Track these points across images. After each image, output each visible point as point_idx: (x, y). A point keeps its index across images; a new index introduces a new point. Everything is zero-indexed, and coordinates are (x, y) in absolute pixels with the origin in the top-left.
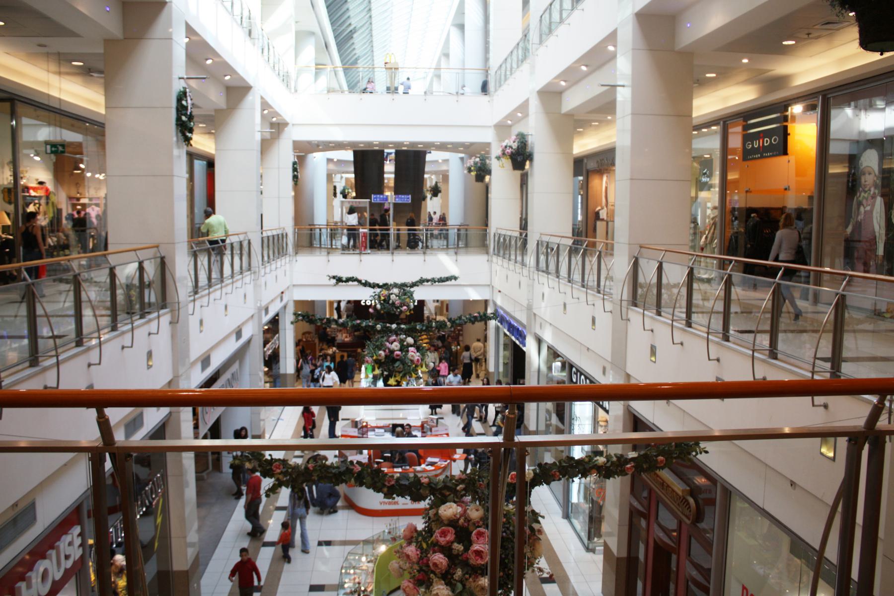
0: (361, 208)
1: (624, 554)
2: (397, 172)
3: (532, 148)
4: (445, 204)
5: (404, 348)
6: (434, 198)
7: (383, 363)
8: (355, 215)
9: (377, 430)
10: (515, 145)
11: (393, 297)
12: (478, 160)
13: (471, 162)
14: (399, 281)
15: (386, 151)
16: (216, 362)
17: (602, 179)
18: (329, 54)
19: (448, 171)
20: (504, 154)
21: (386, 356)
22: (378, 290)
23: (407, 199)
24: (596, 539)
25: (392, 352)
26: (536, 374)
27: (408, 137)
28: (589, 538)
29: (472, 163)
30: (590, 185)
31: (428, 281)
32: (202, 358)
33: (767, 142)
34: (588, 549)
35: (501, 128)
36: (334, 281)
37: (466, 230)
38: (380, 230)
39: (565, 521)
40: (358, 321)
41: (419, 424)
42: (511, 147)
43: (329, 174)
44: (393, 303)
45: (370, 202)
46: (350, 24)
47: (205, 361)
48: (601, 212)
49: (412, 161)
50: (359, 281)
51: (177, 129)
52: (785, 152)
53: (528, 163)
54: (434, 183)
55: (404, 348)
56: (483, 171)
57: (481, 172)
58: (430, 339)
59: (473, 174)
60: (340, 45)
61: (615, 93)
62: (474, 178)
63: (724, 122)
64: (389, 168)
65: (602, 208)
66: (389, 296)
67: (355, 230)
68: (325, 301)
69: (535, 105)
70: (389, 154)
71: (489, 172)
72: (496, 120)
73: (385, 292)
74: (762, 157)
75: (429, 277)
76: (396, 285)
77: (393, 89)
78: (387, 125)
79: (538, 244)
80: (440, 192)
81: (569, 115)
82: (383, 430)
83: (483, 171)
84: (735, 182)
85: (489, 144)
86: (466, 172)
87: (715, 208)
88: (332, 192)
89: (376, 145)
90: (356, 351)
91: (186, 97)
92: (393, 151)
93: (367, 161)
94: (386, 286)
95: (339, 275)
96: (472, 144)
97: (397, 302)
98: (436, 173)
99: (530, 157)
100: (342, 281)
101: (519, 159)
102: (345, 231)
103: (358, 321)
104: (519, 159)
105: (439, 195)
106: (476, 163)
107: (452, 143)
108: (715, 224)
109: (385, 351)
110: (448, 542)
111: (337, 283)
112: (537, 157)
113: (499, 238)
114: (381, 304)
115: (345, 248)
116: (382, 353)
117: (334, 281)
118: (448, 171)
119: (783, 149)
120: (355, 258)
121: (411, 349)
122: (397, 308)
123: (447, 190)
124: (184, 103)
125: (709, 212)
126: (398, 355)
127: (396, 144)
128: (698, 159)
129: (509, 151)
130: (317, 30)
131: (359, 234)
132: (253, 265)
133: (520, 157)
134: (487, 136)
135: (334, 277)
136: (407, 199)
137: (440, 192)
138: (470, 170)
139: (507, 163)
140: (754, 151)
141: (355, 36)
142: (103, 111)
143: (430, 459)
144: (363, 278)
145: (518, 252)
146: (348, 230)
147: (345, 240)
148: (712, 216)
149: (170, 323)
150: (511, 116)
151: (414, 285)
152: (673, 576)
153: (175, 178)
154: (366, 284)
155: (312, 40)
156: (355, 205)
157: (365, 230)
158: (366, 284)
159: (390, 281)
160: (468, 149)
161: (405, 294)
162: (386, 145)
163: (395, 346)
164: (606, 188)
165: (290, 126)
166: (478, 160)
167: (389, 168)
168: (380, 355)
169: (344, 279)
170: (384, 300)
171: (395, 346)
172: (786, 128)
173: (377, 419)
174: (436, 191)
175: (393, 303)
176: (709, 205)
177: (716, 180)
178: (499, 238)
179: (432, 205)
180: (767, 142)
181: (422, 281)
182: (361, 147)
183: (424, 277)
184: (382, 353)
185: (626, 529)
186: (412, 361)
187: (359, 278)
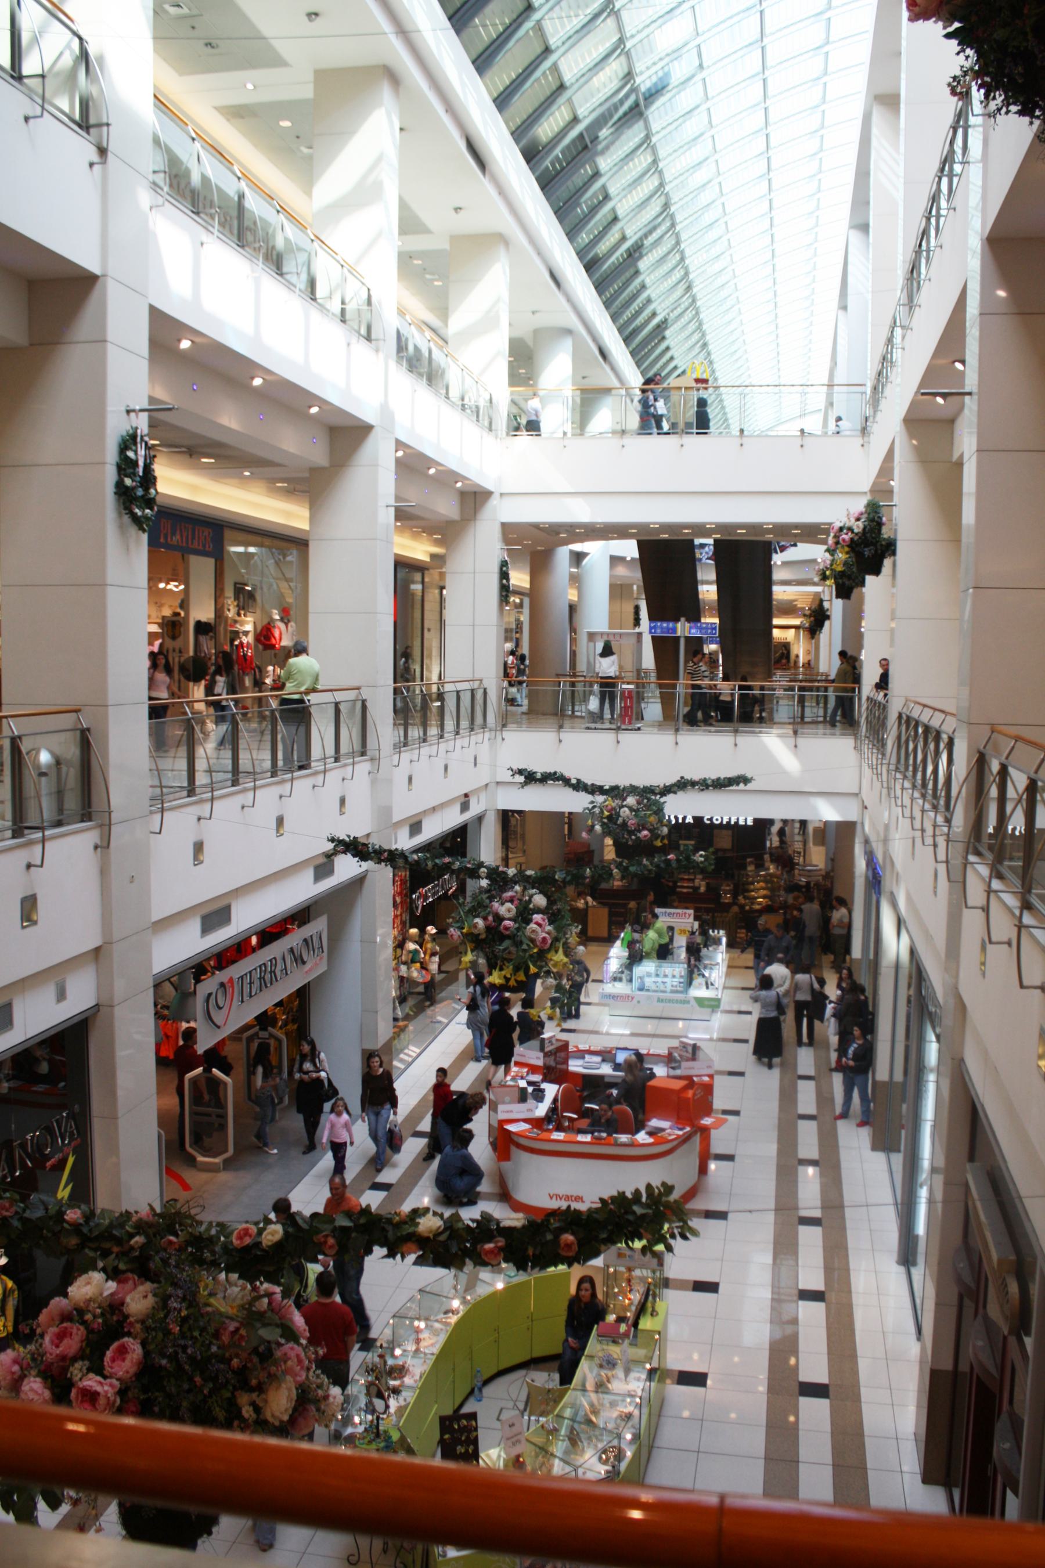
5: (524, 915)
7: (483, 940)
9: (588, 1057)
14: (641, 782)
15: (697, 541)
16: (248, 916)
18: (613, 369)
21: (488, 928)
22: (600, 799)
26: (893, 971)
31: (693, 784)
32: (206, 910)
36: (522, 779)
39: (902, 1269)
40: (447, 860)
41: (665, 1052)
42: (850, 529)
43: (598, 582)
44: (624, 824)
46: (654, 314)
47: (215, 916)
49: (746, 558)
50: (567, 782)
51: (118, 500)
55: (524, 915)
58: (772, 890)
68: (563, 813)
70: (702, 546)
73: (612, 803)
75: (696, 778)
76: (633, 790)
80: (828, 617)
82: (598, 1059)
89: (768, 531)
90: (625, 905)
91: (135, 444)
92: (711, 541)
93: (665, 563)
94: (615, 792)
95: (532, 767)
97: (632, 822)
100: (536, 780)
101: (867, 552)
102: (596, 687)
103: (447, 860)
104: (867, 552)
109: (485, 919)
110: (63, 1358)
111: (523, 785)
114: (603, 825)
115: (597, 717)
117: (522, 779)
120: (609, 737)
121: (537, 917)
122: (631, 833)
124: (130, 454)
126: (507, 928)
129: (846, 537)
132: (369, 745)
135: (520, 772)
141: (667, 333)
143: (655, 1123)
144: (572, 774)
146: (602, 685)
147: (594, 704)
149: (96, 847)
151: (667, 790)
153: (110, 589)
154: (579, 786)
155: (568, 343)
158: (579, 786)
159: (623, 782)
161: (648, 807)
162: (701, 529)
163: (506, 909)
165: (494, 501)
168: (475, 926)
169: (539, 776)
170: (609, 818)
171: (506, 909)
173: (633, 1035)
175: (624, 824)
181: (682, 785)
183: (688, 777)
184: (480, 922)
186: (533, 941)
187: (567, 774)
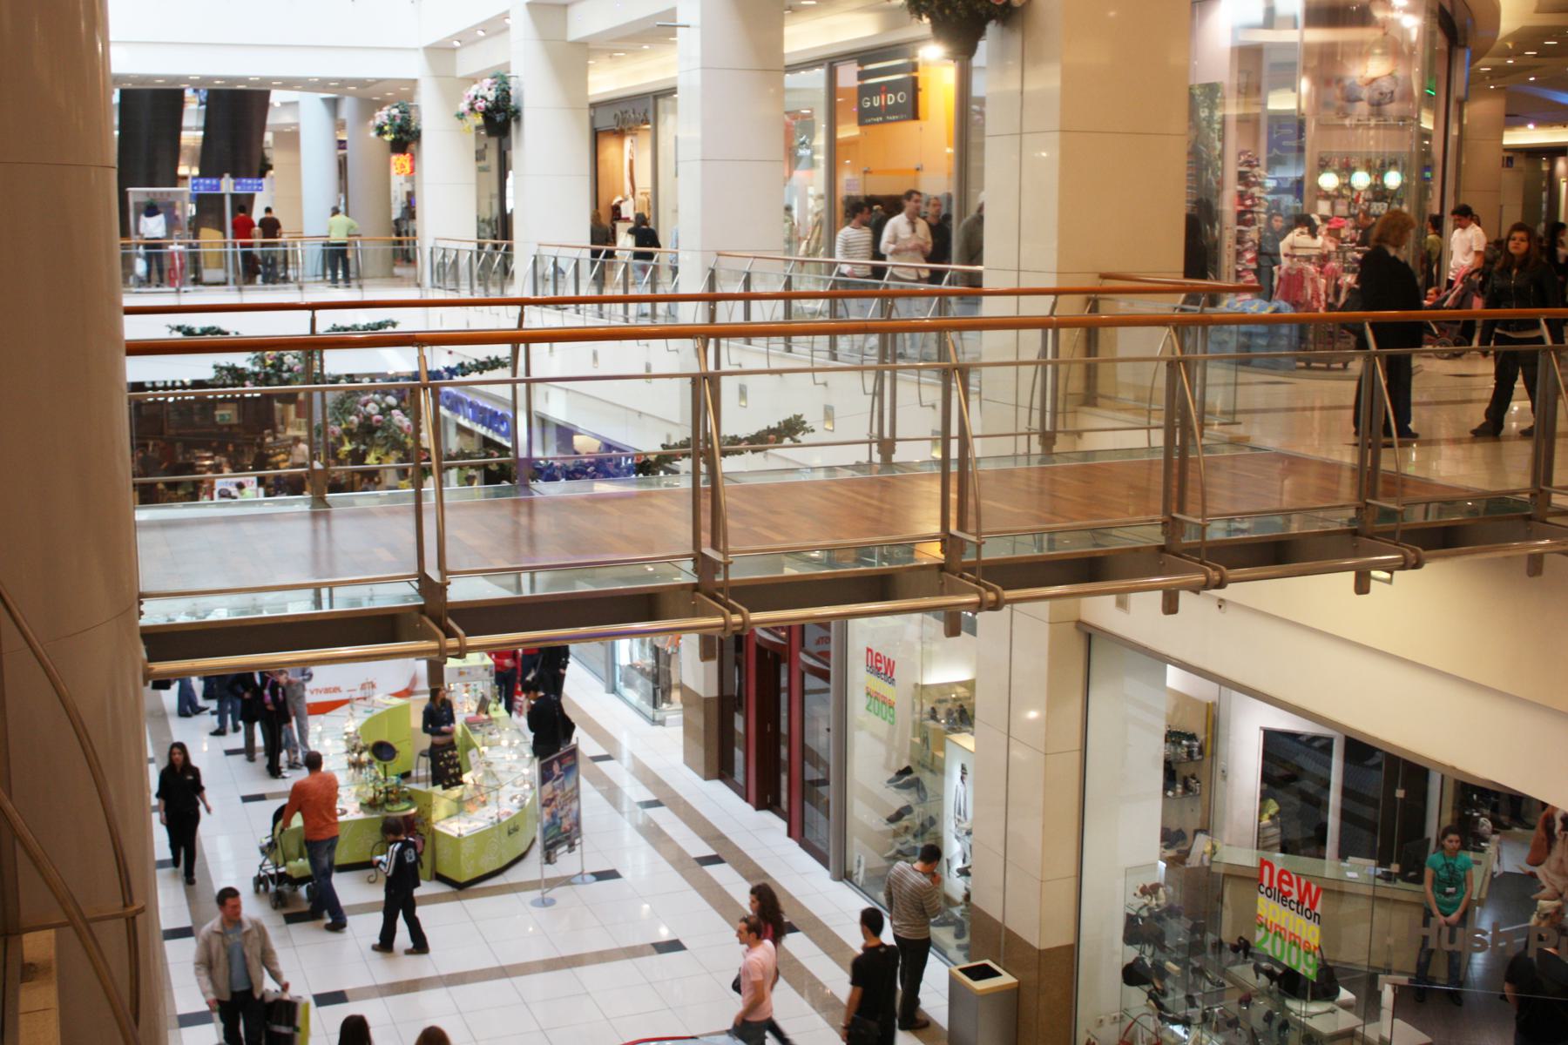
1: (714, 693)
2: (177, 128)
3: (519, 98)
10: (491, 95)
13: (381, 116)
17: (622, 146)
20: (472, 109)
24: (665, 705)
25: (368, 417)
28: (655, 705)
30: (601, 157)
33: (891, 99)
34: (654, 722)
35: (440, 53)
38: (263, 245)
39: (612, 696)
42: (484, 98)
48: (623, 206)
52: (915, 116)
57: (405, 138)
62: (388, 147)
63: (831, 64)
65: (626, 199)
67: (159, 246)
74: (885, 121)
79: (535, 262)
80: (270, 167)
83: (407, 132)
84: (851, 142)
85: (414, 82)
87: (821, 197)
99: (516, 114)
102: (141, 250)
106: (392, 118)
108: (819, 223)
112: (527, 116)
116: (353, 418)
119: (912, 111)
123: (297, 165)
125: (811, 203)
127: (205, 80)
128: (794, 114)
129: (481, 104)
133: (499, 120)
134: (410, 67)
138: (381, 131)
140: (873, 112)
145: (476, 283)
146: (147, 246)
148: (816, 210)
152: (783, 740)
157: (181, 248)
160: (369, 96)
163: (372, 408)
164: (631, 162)
166: (395, 112)
170: (272, 366)
172: (915, 80)
176: (811, 191)
177: (820, 140)
180: (891, 99)
182: (129, 86)
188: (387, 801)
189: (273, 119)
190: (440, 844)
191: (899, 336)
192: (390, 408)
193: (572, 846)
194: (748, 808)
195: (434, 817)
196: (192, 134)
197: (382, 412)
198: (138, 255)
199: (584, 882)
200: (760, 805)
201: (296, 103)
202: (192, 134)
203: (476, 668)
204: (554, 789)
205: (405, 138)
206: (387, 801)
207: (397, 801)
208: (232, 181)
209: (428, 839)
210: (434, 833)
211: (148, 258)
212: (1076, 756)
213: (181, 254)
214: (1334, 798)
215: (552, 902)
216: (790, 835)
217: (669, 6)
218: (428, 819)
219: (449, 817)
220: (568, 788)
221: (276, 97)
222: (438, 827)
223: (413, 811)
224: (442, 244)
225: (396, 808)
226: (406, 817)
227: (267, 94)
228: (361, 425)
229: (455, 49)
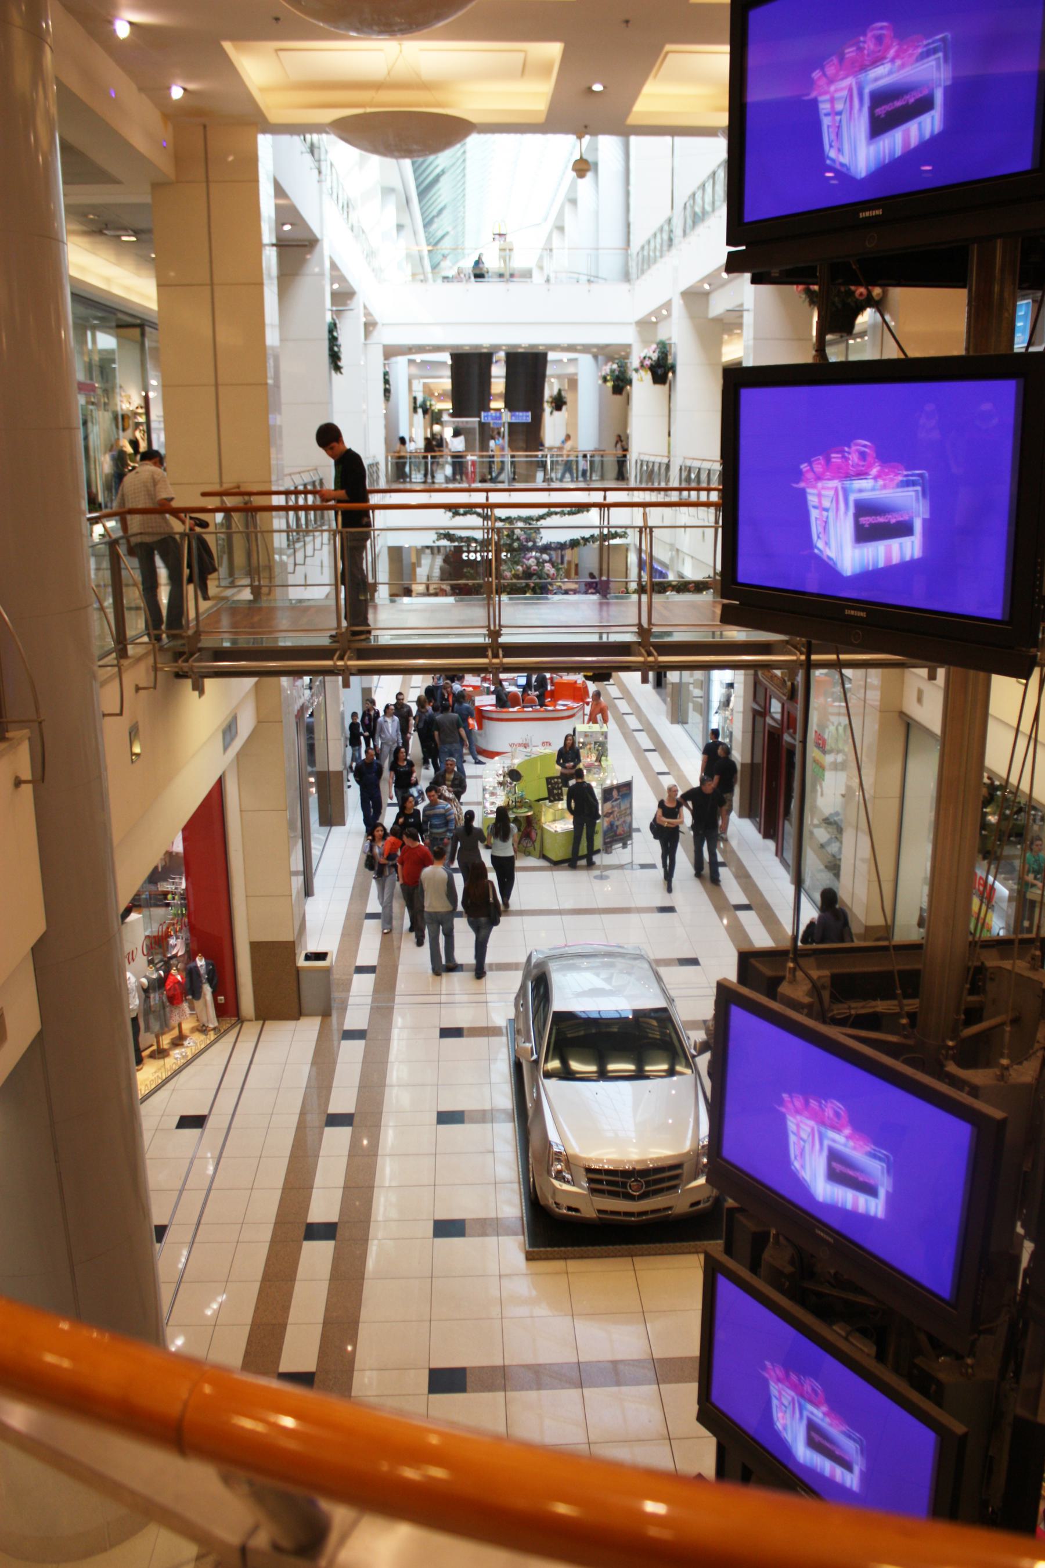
0: (469, 429)
1: (748, 760)
3: (675, 359)
4: (573, 422)
5: (540, 563)
6: (556, 413)
8: (462, 438)
11: (517, 532)
12: (615, 366)
13: (607, 369)
19: (576, 374)
20: (642, 366)
23: (526, 417)
25: (529, 568)
27: (525, 339)
29: (608, 371)
35: (645, 325)
37: (602, 456)
42: (650, 358)
45: (480, 422)
49: (528, 368)
53: (670, 375)
54: (555, 392)
56: (622, 381)
57: (620, 384)
59: (610, 384)
60: (422, 194)
61: (741, 317)
62: (610, 390)
64: (498, 372)
66: (513, 532)
69: (678, 305)
71: (630, 382)
72: (640, 315)
77: (507, 275)
78: (496, 323)
80: (565, 403)
81: (718, 320)
85: (629, 346)
86: (600, 382)
88: (412, 405)
93: (469, 368)
96: (607, 346)
97: (523, 537)
98: (559, 377)
99: (673, 368)
101: (660, 371)
102: (449, 459)
104: (660, 371)
105: (564, 408)
106: (612, 371)
107: (583, 345)
113: (642, 465)
116: (520, 568)
118: (576, 374)
123: (576, 401)
129: (648, 362)
130: (399, 186)
131: (467, 462)
133: (661, 371)
134: (625, 335)
136: (526, 417)
137: (565, 403)
138: (605, 380)
139: (648, 376)
142: (154, 306)
146: (453, 457)
150: (656, 312)
156: (461, 425)
157: (474, 458)
160: (602, 352)
162: (497, 348)
163: (532, 562)
165: (379, 326)
166: (615, 366)
167: (498, 372)
171: (532, 562)
174: (559, 403)
178: (642, 465)
179: (553, 427)
185: (749, 735)
188: (515, 807)
189: (550, 370)
190: (546, 836)
191: (326, 512)
192: (545, 561)
193: (625, 846)
194: (759, 837)
195: (543, 819)
196: (498, 384)
197: (538, 564)
198: (447, 462)
199: (632, 868)
200: (767, 835)
201: (576, 360)
202: (498, 384)
203: (596, 733)
204: (613, 807)
205: (621, 384)
206: (515, 807)
207: (521, 807)
208: (509, 414)
209: (539, 832)
210: (542, 829)
211: (454, 465)
212: (896, 802)
213: (474, 463)
214: (18, 639)
215: (607, 877)
216: (777, 854)
217: (739, 303)
218: (540, 820)
219: (555, 820)
220: (623, 807)
221: (551, 356)
222: (545, 826)
223: (530, 814)
224: (688, 463)
225: (519, 811)
226: (528, 817)
227: (545, 355)
228: (524, 572)
229: (707, 294)
